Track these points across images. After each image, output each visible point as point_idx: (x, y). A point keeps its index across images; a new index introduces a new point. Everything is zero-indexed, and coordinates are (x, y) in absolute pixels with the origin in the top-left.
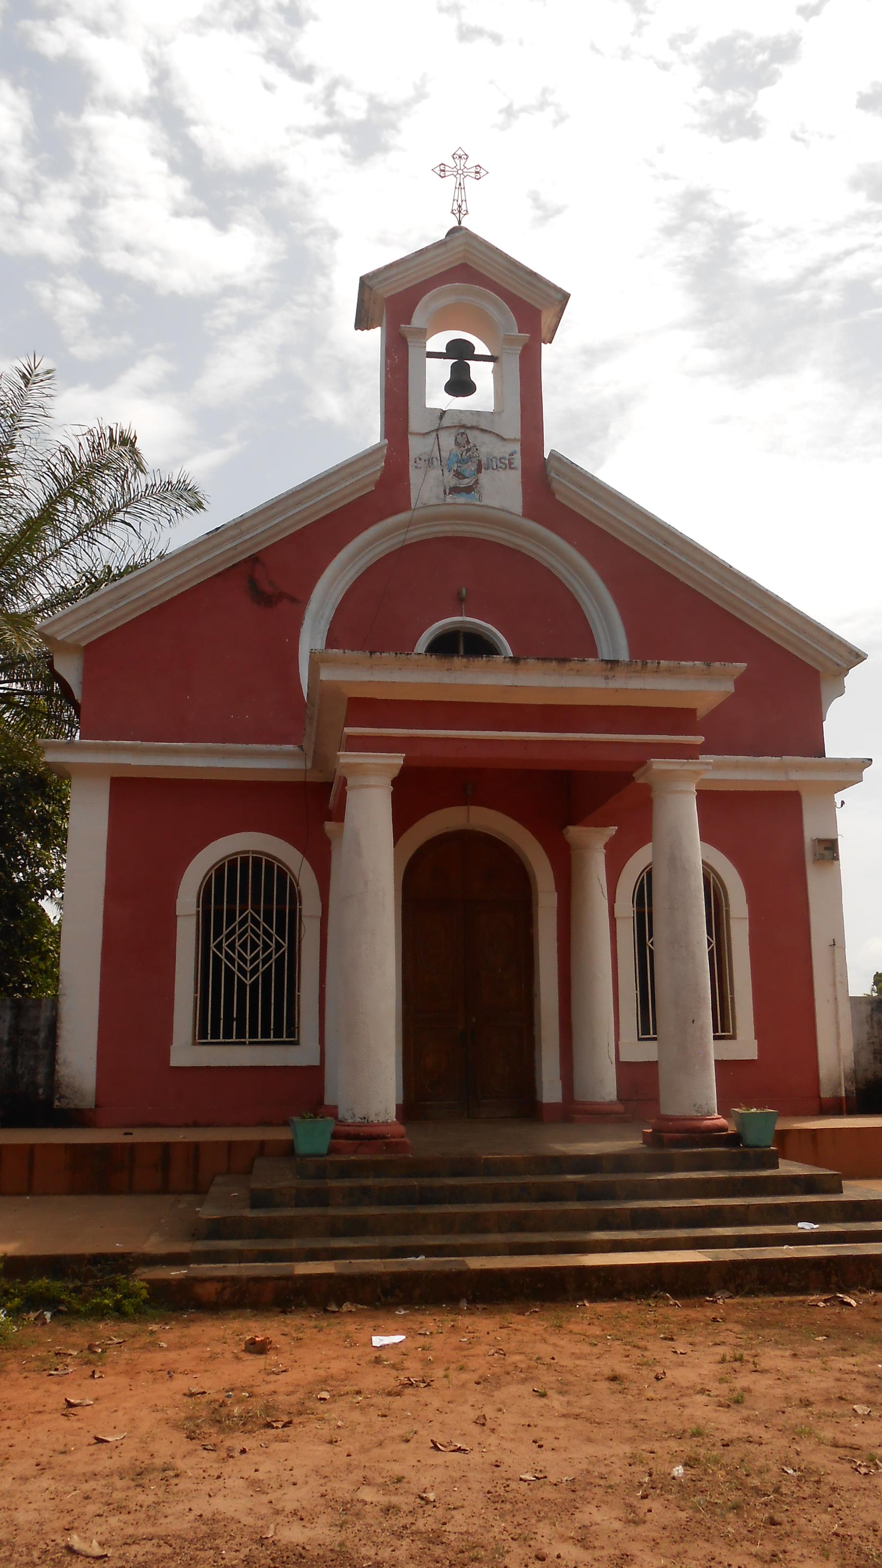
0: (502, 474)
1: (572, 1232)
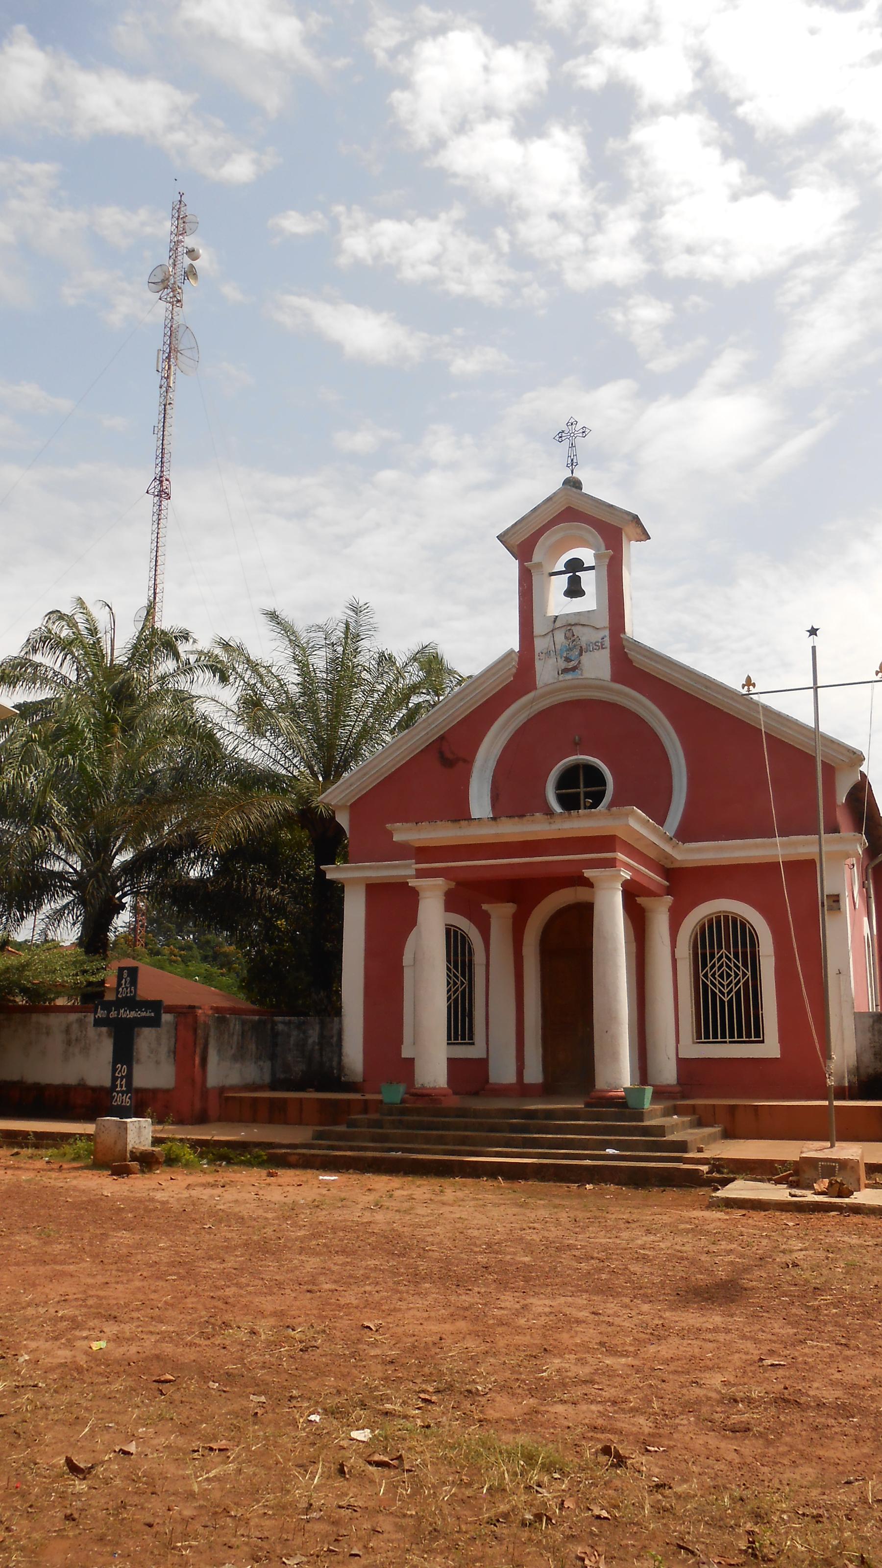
0: (596, 653)
1: (477, 1146)
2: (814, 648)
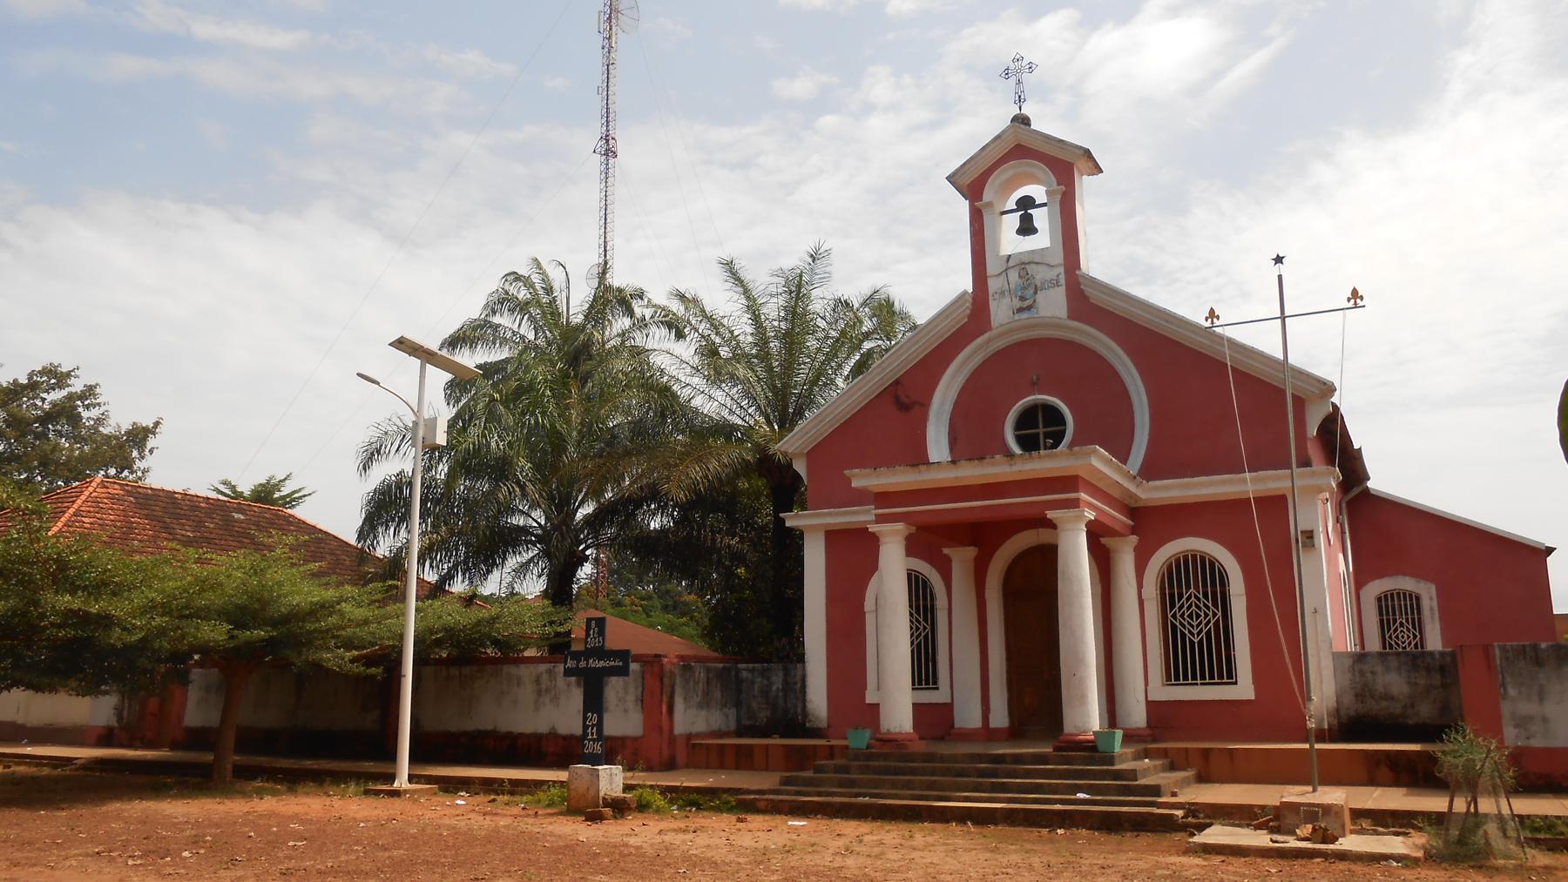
2: (1280, 277)
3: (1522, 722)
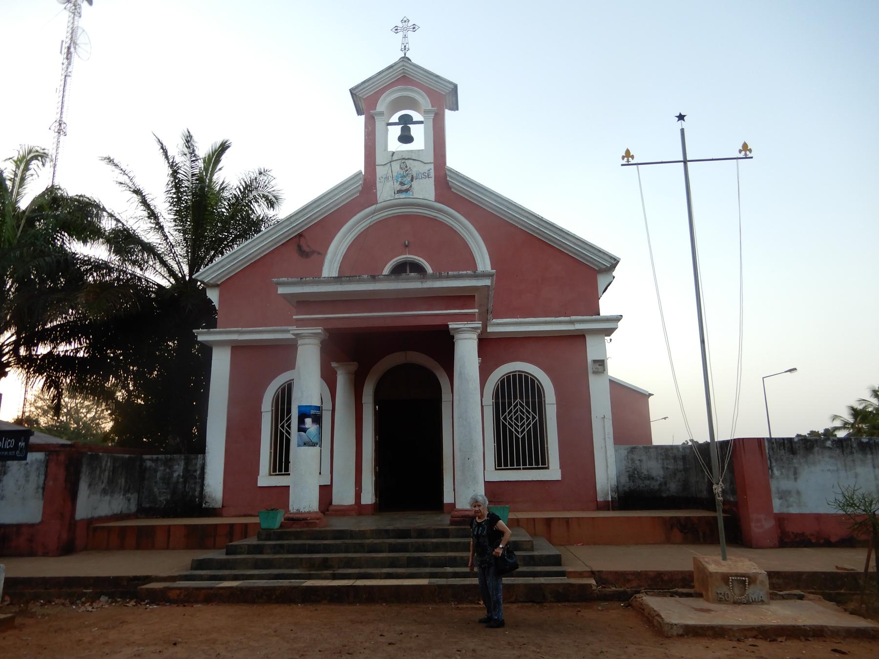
2: (682, 131)
3: (784, 495)
